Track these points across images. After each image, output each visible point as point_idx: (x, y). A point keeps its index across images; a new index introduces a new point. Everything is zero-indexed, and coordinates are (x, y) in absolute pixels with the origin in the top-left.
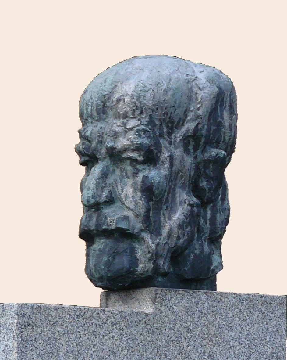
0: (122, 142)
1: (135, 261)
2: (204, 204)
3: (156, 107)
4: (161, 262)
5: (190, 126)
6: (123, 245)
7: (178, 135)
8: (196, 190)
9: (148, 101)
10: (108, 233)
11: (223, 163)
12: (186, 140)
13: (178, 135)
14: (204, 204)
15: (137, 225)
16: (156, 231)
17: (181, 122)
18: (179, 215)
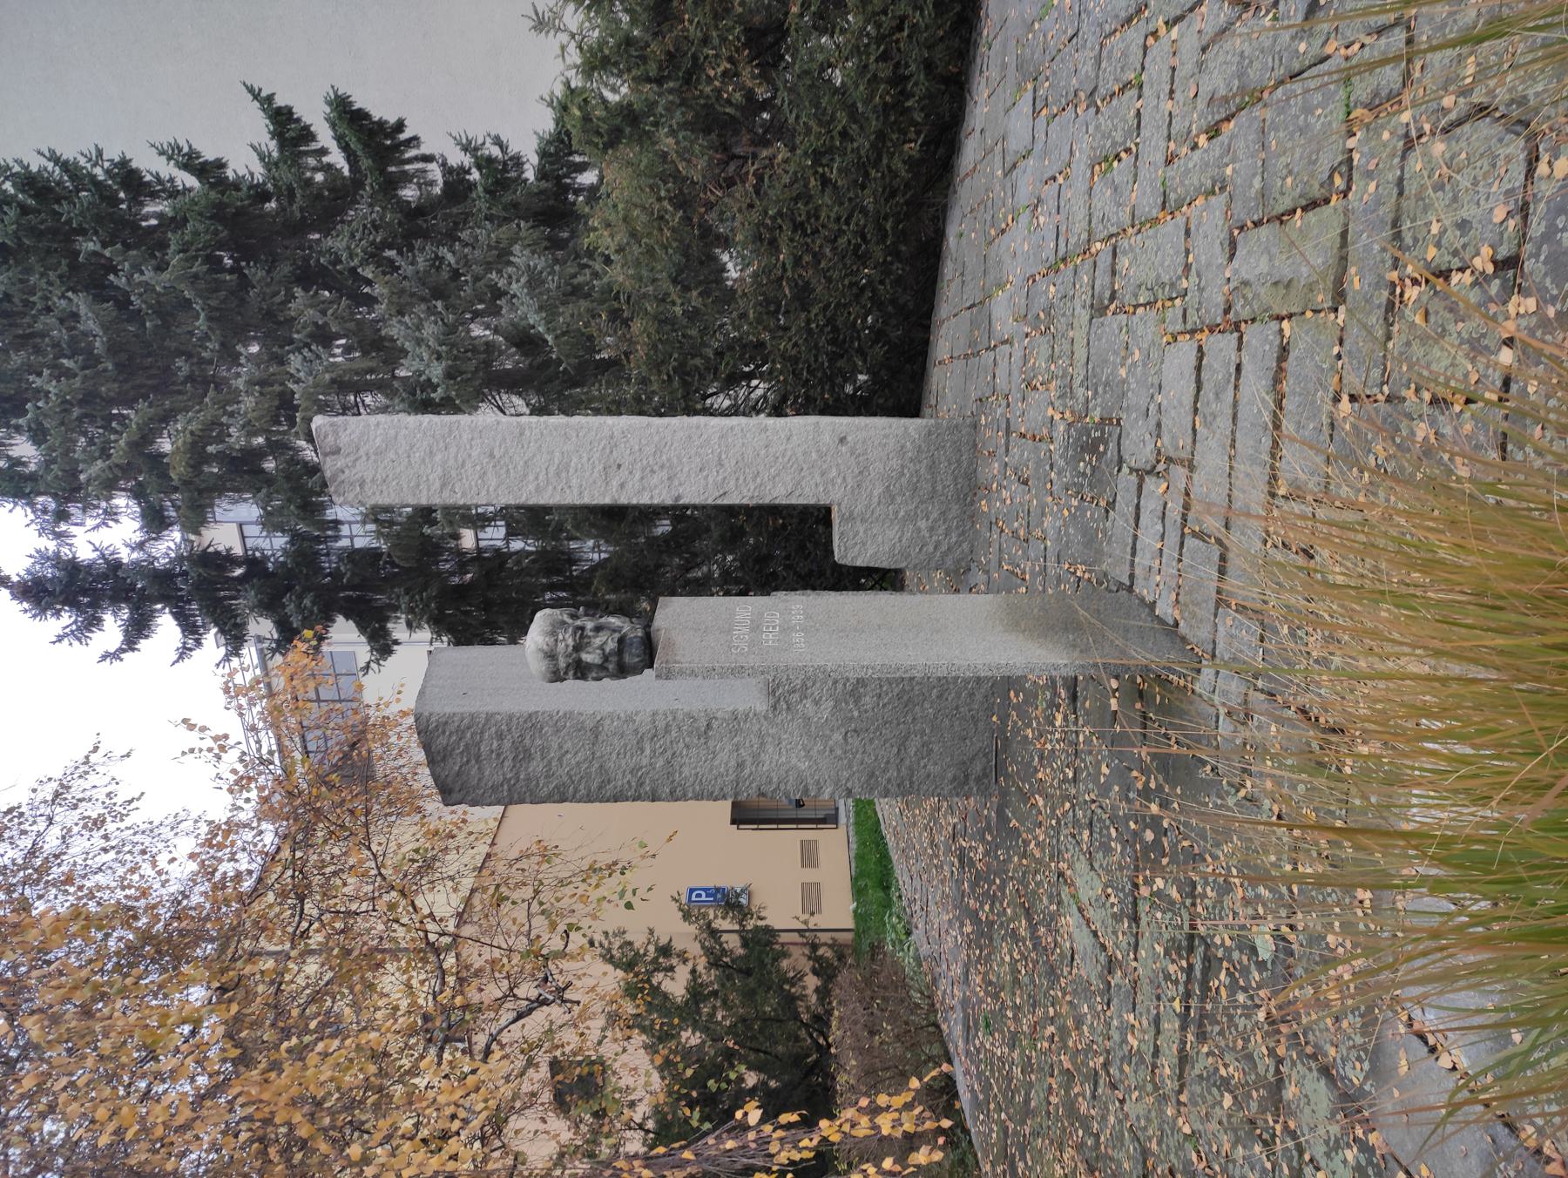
0: (570, 642)
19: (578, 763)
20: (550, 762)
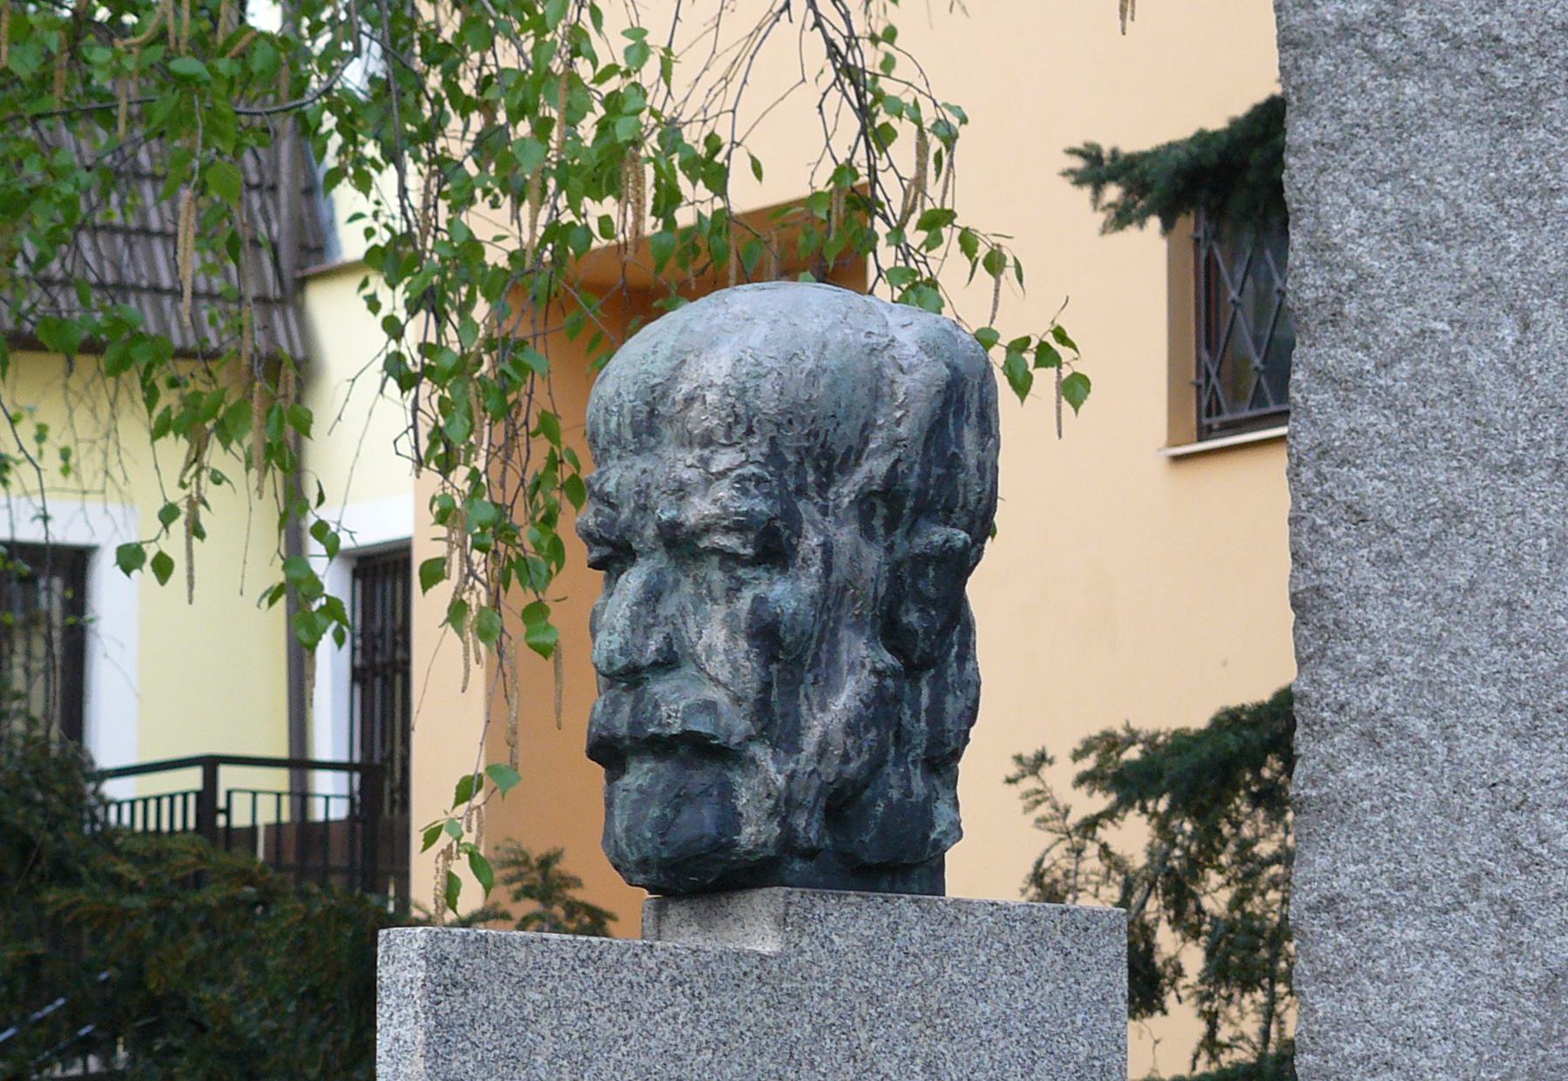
1: (731, 820)
2: (912, 670)
3: (788, 417)
4: (800, 821)
5: (875, 467)
6: (701, 778)
7: (846, 490)
8: (890, 633)
9: (767, 401)
10: (661, 746)
11: (961, 563)
12: (865, 503)
13: (846, 490)
14: (912, 670)
15: (739, 725)
16: (785, 738)
17: (853, 456)
18: (846, 698)
19: (1466, 389)
20: (1474, 232)
